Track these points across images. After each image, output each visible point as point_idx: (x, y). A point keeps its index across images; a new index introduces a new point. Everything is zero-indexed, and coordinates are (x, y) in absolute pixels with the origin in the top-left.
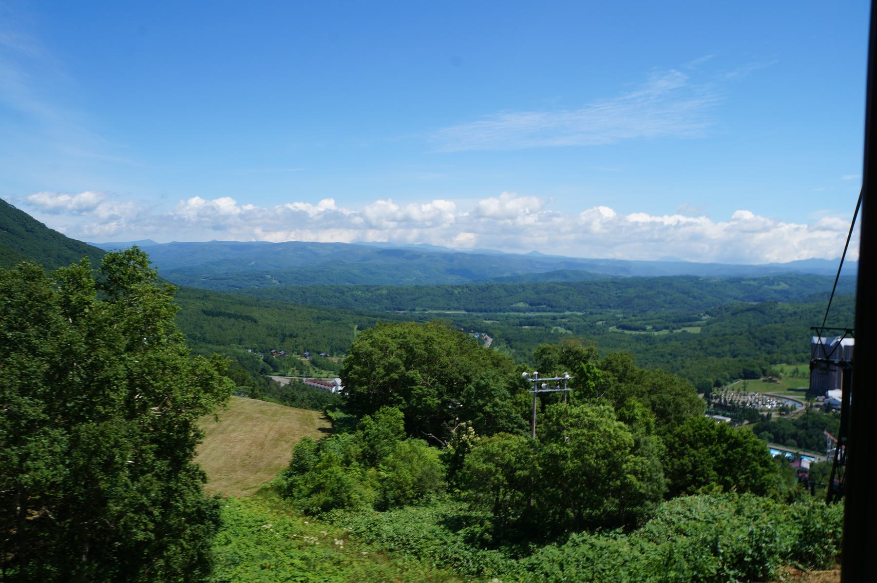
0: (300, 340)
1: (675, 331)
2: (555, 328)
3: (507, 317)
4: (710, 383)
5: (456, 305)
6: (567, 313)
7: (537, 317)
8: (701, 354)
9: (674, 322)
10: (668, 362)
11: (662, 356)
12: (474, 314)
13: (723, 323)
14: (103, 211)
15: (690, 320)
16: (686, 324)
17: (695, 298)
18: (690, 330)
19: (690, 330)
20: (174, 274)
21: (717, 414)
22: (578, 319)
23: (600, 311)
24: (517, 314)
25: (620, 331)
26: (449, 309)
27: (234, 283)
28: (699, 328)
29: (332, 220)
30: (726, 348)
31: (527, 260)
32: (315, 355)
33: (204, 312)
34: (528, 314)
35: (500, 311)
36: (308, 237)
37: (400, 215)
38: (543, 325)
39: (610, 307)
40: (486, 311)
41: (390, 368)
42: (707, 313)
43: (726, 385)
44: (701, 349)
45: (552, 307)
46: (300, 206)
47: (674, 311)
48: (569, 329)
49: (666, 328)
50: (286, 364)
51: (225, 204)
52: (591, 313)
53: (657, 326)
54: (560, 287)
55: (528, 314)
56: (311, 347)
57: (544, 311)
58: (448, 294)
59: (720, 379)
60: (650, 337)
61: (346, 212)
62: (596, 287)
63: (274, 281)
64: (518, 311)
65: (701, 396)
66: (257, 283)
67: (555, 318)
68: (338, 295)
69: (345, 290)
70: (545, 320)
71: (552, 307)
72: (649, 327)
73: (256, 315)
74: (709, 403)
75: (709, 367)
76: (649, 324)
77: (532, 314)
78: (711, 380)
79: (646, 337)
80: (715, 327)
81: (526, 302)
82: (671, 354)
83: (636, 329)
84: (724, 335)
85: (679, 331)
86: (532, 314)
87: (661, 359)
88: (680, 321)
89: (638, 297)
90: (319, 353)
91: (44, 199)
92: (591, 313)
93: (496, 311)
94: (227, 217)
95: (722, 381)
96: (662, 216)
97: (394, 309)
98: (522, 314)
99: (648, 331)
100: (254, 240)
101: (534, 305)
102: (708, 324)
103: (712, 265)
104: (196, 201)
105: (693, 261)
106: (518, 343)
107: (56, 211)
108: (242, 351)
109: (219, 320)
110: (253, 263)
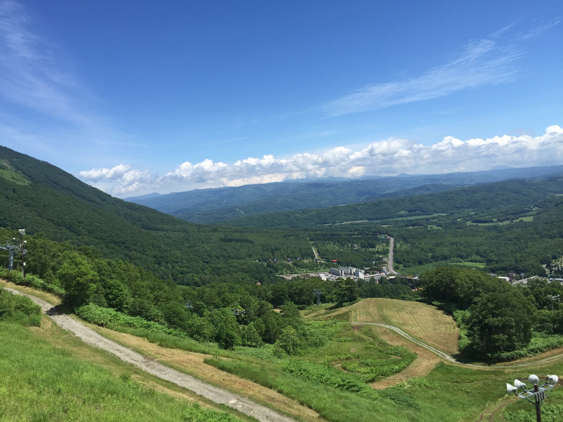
0: (283, 251)
1: (514, 221)
2: (430, 226)
3: (396, 222)
4: (549, 257)
5: (360, 217)
6: (435, 215)
7: (416, 220)
8: (538, 236)
9: (512, 214)
10: (515, 244)
11: (510, 240)
12: (375, 222)
13: (549, 213)
14: (129, 176)
15: (524, 212)
16: (521, 215)
17: (524, 195)
18: (525, 219)
19: (525, 219)
20: (178, 214)
21: (558, 277)
22: (444, 218)
23: (458, 211)
24: (401, 219)
25: (475, 224)
26: (357, 220)
27: (217, 216)
28: (532, 217)
29: (275, 168)
30: (556, 231)
31: (404, 180)
32: (294, 260)
33: (221, 240)
34: (409, 218)
35: (390, 218)
36: (255, 180)
37: (320, 160)
38: (422, 225)
39: (464, 208)
40: (381, 219)
41: (469, 288)
42: (536, 206)
43: (560, 257)
44: (537, 233)
45: (424, 212)
46: (252, 161)
47: (511, 206)
48: (440, 226)
49: (508, 219)
50: (280, 267)
51: (207, 164)
52: (452, 214)
53: (501, 218)
54: (427, 198)
55: (409, 218)
56: (291, 255)
57: (419, 215)
58: (353, 211)
59: (555, 254)
60: (498, 227)
61: (283, 161)
62: (451, 195)
63: (242, 212)
64: (402, 217)
65: (544, 266)
66: (231, 214)
67: (428, 219)
68: (285, 218)
69: (290, 214)
70: (422, 221)
71: (424, 212)
72: (495, 220)
73: (250, 237)
74: (551, 271)
75: (546, 246)
76: (494, 218)
77: (411, 218)
78: (550, 256)
79: (495, 227)
80: (544, 216)
81: (406, 210)
82: (516, 239)
83: (486, 222)
84: (552, 222)
85: (518, 221)
86: (411, 218)
87: (510, 242)
88: (516, 213)
89: (483, 199)
90: (296, 258)
91: (94, 173)
92: (452, 214)
93: (387, 218)
94: (209, 173)
95: (557, 255)
96: (492, 138)
97: (322, 223)
98: (405, 219)
99: (495, 222)
100: (222, 186)
101: (412, 212)
102: (538, 214)
103: (533, 168)
104: (186, 165)
105: (517, 167)
106: (411, 240)
107: (95, 180)
108: (254, 262)
109: (232, 244)
110: (225, 201)
